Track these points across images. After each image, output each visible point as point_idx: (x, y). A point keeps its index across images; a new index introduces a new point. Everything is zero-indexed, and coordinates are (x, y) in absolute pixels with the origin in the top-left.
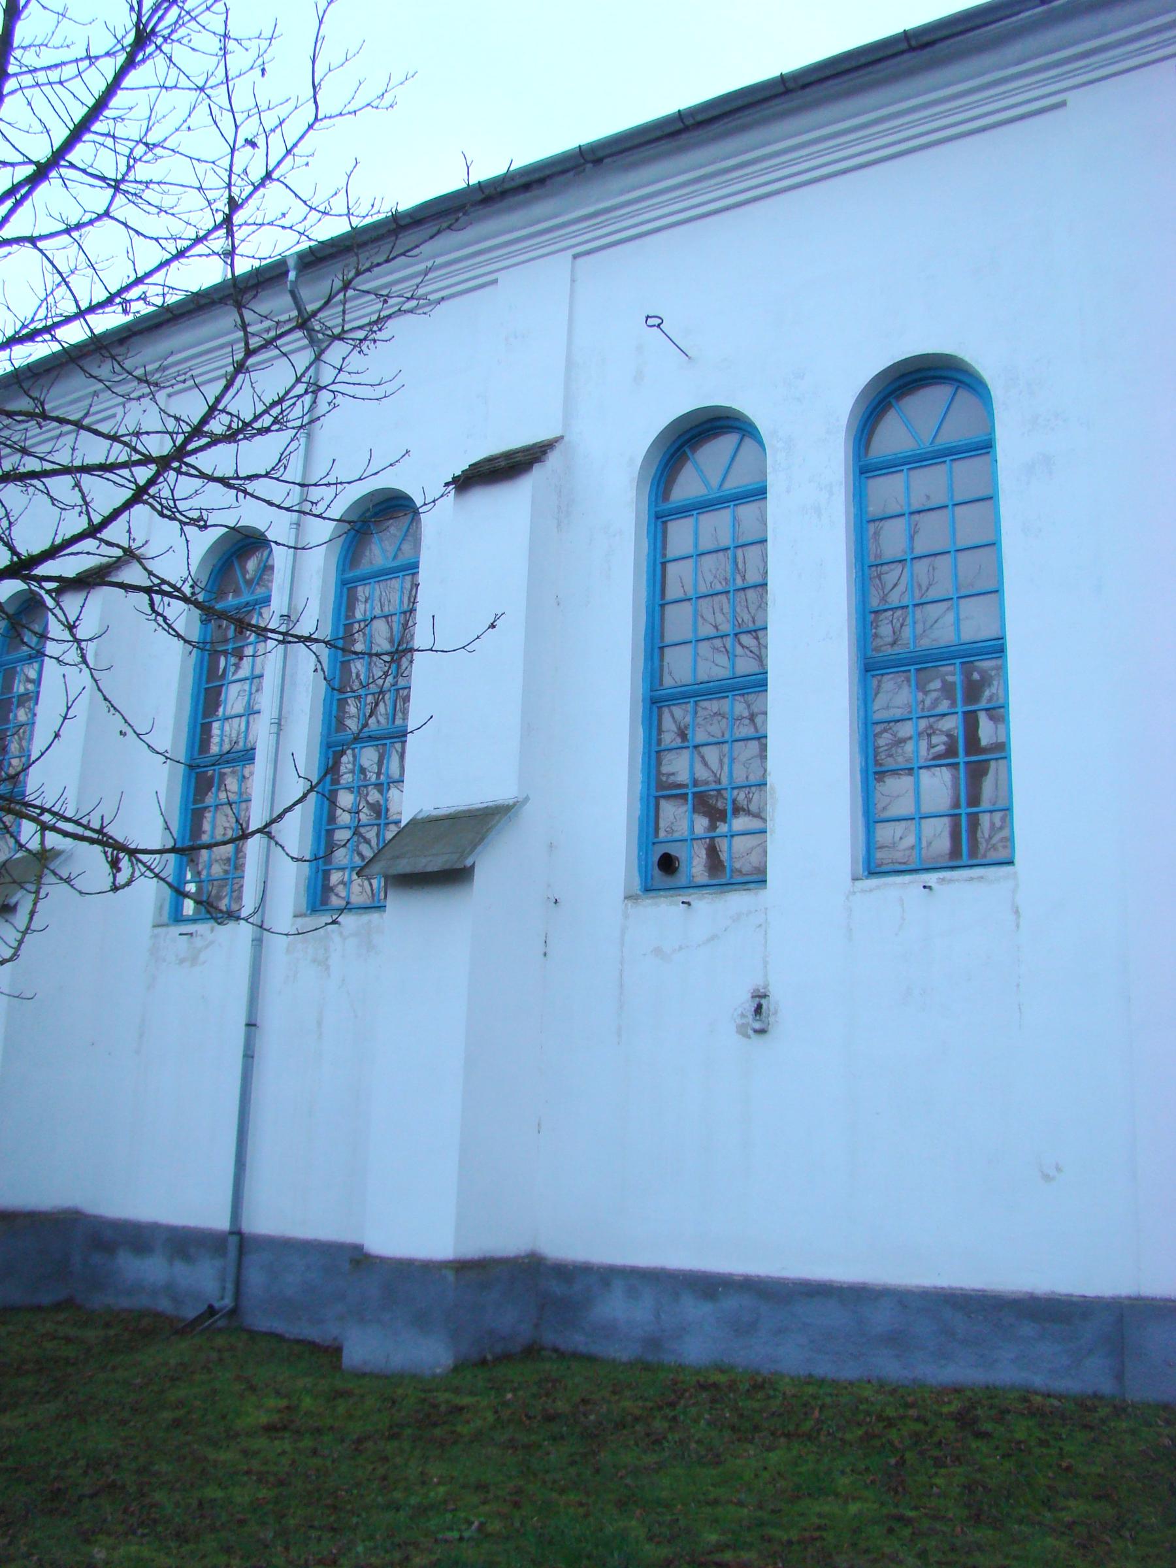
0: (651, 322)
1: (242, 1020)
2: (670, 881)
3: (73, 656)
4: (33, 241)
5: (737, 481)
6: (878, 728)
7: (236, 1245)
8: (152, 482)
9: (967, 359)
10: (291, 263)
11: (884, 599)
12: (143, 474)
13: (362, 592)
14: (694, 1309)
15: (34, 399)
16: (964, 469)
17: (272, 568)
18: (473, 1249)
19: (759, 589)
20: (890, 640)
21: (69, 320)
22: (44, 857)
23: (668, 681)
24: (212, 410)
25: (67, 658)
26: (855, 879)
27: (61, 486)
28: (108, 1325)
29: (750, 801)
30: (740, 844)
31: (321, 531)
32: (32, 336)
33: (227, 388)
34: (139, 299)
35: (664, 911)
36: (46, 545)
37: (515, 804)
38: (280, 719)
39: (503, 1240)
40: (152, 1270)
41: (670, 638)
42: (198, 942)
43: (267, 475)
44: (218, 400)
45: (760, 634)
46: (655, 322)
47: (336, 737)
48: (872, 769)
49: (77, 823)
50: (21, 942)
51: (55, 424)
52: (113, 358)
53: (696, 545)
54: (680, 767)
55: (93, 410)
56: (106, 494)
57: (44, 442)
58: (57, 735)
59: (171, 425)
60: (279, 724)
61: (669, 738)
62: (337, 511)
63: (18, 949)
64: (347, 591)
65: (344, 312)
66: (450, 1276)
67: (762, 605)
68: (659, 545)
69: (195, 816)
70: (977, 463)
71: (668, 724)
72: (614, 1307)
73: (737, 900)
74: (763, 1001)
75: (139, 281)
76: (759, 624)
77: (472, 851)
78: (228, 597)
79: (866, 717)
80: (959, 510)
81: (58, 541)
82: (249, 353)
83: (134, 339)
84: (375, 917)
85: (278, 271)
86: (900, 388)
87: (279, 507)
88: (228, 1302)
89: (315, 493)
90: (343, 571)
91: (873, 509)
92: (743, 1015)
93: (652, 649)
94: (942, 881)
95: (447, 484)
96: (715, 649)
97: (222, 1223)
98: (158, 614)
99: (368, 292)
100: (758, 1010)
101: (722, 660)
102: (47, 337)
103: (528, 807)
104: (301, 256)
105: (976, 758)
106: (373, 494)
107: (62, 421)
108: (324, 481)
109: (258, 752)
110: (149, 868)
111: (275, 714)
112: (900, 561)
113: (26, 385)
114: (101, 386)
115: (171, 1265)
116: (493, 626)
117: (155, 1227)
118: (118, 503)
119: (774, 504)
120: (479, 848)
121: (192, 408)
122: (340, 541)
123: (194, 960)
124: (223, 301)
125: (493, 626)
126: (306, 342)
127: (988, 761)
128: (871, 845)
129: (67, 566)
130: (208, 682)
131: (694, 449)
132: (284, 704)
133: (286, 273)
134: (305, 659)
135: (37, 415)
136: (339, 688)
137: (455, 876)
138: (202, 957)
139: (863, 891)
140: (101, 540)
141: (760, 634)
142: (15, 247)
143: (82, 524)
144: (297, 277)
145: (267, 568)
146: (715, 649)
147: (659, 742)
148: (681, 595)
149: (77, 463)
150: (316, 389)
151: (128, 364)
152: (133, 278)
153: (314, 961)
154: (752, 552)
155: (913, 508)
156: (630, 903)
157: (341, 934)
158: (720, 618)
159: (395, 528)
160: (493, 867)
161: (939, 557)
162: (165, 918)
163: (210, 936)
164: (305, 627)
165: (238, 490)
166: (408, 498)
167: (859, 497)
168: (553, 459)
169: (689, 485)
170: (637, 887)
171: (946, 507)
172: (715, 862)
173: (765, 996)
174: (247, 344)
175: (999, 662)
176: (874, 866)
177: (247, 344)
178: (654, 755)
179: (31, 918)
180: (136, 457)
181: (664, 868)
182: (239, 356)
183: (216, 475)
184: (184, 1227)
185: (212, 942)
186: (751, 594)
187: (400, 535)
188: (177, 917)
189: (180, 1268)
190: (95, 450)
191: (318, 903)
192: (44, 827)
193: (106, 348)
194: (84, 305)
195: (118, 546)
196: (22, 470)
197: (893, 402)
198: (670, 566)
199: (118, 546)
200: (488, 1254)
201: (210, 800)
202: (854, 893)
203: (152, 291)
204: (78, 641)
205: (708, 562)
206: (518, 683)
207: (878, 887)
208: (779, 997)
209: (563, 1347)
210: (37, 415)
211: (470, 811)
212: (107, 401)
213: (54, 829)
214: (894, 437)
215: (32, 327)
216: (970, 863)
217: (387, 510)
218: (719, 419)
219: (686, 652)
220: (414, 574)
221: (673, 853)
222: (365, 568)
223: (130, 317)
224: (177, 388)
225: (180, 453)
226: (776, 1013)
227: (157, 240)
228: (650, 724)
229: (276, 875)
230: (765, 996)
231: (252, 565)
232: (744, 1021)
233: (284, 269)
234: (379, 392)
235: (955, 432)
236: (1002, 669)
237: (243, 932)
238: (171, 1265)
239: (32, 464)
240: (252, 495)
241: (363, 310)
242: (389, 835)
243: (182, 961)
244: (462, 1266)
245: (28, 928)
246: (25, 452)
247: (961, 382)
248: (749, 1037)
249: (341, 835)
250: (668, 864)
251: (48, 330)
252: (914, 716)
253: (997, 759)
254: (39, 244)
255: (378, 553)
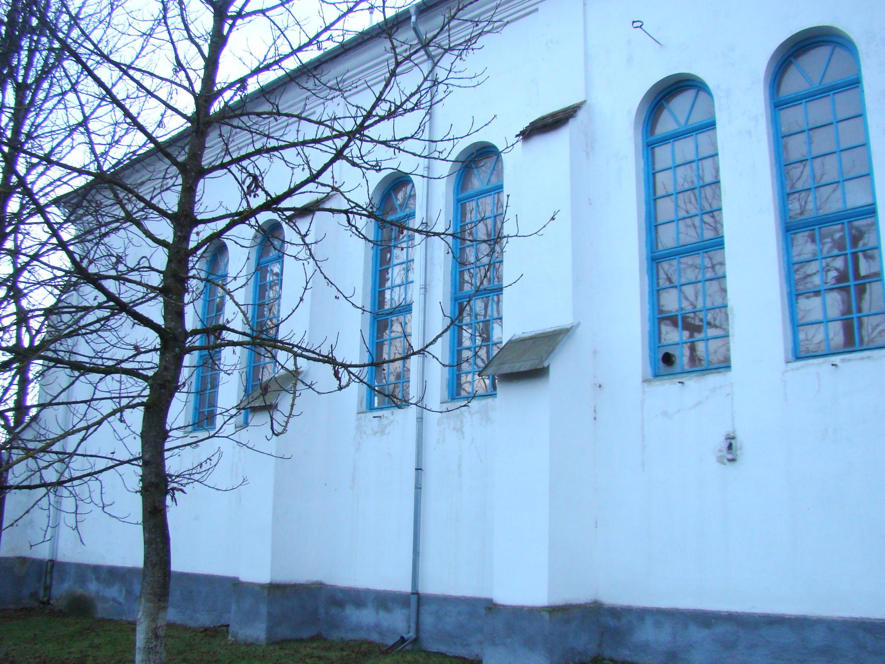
0: (636, 25)
1: (413, 466)
2: (669, 370)
3: (304, 254)
4: (263, 12)
5: (697, 118)
6: (796, 266)
7: (416, 601)
8: (346, 146)
9: (840, 28)
10: (412, 11)
11: (793, 186)
12: (340, 143)
13: (470, 205)
14: (696, 633)
15: (272, 104)
16: (841, 98)
17: (415, 195)
18: (559, 600)
19: (714, 186)
20: (798, 211)
21: (287, 56)
22: (295, 374)
23: (660, 248)
24: (379, 99)
25: (300, 256)
26: (787, 362)
27: (290, 154)
28: (342, 649)
29: (715, 319)
30: (713, 345)
31: (443, 168)
32: (268, 67)
33: (386, 86)
34: (328, 39)
35: (668, 390)
36: (286, 189)
37: (572, 327)
38: (425, 285)
39: (578, 594)
40: (367, 616)
41: (660, 220)
42: (385, 421)
43: (412, 137)
44: (381, 94)
45: (716, 214)
46: (638, 24)
47: (459, 294)
48: (794, 293)
49: (313, 352)
50: (287, 423)
51: (286, 118)
52: (314, 76)
53: (674, 162)
54: (671, 302)
55: (307, 108)
56: (318, 157)
57: (279, 130)
58: (301, 299)
59: (353, 111)
60: (425, 288)
61: (663, 282)
62: (453, 157)
63: (286, 426)
64: (461, 204)
65: (449, 36)
66: (546, 616)
67: (718, 196)
68: (650, 163)
69: (378, 346)
70: (850, 94)
71: (662, 275)
72: (647, 633)
73: (713, 380)
74: (733, 441)
75: (327, 29)
76: (715, 207)
77: (547, 358)
78: (389, 213)
79: (788, 260)
80: (841, 125)
81: (292, 186)
82: (398, 64)
83: (323, 66)
84: (490, 401)
85: (404, 17)
86: (797, 51)
87: (420, 156)
88: (412, 634)
89: (440, 146)
90: (457, 194)
91: (784, 130)
92: (720, 451)
93: (650, 227)
94: (843, 360)
95: (517, 136)
96: (688, 226)
97: (407, 588)
98: (353, 226)
99: (466, 20)
100: (730, 447)
101: (692, 232)
102: (277, 67)
103: (579, 330)
104: (418, 6)
105: (853, 284)
106: (475, 144)
107: (287, 115)
108: (447, 138)
109: (414, 306)
110: (357, 377)
111: (422, 283)
112: (801, 161)
113: (267, 97)
114: (309, 93)
115: (377, 613)
116: (553, 219)
117: (367, 592)
118: (327, 161)
119: (722, 131)
120: (552, 355)
121: (366, 100)
122: (455, 174)
123: (383, 432)
124: (378, 35)
125: (553, 219)
126: (426, 57)
127: (864, 284)
128: (795, 342)
129: (298, 201)
130: (381, 266)
131: (668, 101)
132: (427, 275)
133: (410, 17)
134: (440, 249)
135: (274, 114)
136: (460, 262)
137: (538, 373)
138: (387, 431)
139: (793, 369)
140: (318, 183)
141: (716, 214)
142: (254, 16)
143: (306, 175)
144: (417, 19)
145: (413, 196)
146: (688, 226)
147: (658, 285)
148: (664, 193)
149: (301, 139)
150: (436, 83)
151: (324, 79)
152: (323, 27)
153: (455, 429)
154: (707, 164)
155: (811, 126)
156: (646, 384)
157: (470, 412)
158: (689, 207)
159: (488, 164)
160: (560, 367)
161: (828, 157)
162: (364, 408)
163: (391, 418)
164: (440, 228)
165: (395, 148)
166: (494, 147)
167: (775, 123)
168: (581, 115)
169: (666, 125)
170: (649, 373)
171: (831, 124)
172: (694, 358)
173: (733, 438)
174: (396, 58)
175: (873, 219)
176: (799, 353)
177: (396, 58)
178: (655, 293)
179: (292, 409)
180: (334, 133)
181: (665, 362)
182: (392, 67)
183: (381, 139)
184: (384, 591)
185: (392, 422)
186: (708, 191)
187: (489, 171)
188: (371, 408)
189: (382, 614)
190: (309, 131)
191: (455, 394)
192: (296, 355)
193: (309, 71)
194: (295, 47)
195: (329, 186)
196: (269, 146)
197: (793, 60)
198: (658, 176)
199: (329, 186)
200: (569, 602)
201: (387, 335)
202: (787, 371)
203: (335, 33)
204: (307, 245)
205: (680, 171)
206: (571, 252)
207: (802, 367)
208: (743, 439)
209: (616, 658)
210: (274, 114)
211: (544, 333)
212: (313, 102)
213: (301, 356)
214: (794, 83)
215: (265, 63)
216: (861, 348)
217: (480, 156)
218: (682, 81)
219: (672, 227)
220: (498, 193)
221: (671, 352)
222: (470, 192)
223: (322, 52)
224: (353, 91)
225: (361, 128)
226: (741, 448)
227: (334, 4)
228: (652, 273)
229: (429, 376)
230: (733, 438)
231: (400, 196)
232: (722, 454)
233: (408, 15)
234: (474, 82)
235: (834, 76)
236: (874, 225)
237: (412, 412)
238: (377, 613)
239: (273, 143)
240: (403, 151)
241: (460, 33)
242: (495, 353)
243: (375, 433)
244: (553, 610)
245: (291, 414)
246: (268, 137)
247: (837, 43)
248: (725, 464)
249: (466, 354)
250: (668, 359)
251: (276, 63)
252: (819, 257)
253: (870, 282)
254: (267, 14)
255: (477, 183)
